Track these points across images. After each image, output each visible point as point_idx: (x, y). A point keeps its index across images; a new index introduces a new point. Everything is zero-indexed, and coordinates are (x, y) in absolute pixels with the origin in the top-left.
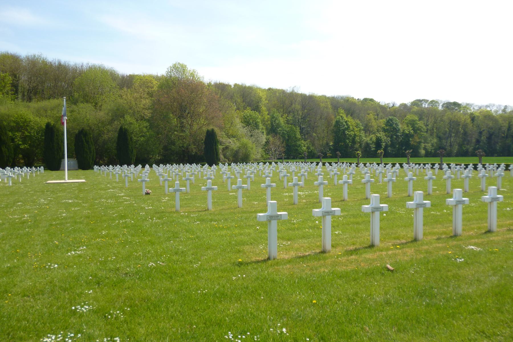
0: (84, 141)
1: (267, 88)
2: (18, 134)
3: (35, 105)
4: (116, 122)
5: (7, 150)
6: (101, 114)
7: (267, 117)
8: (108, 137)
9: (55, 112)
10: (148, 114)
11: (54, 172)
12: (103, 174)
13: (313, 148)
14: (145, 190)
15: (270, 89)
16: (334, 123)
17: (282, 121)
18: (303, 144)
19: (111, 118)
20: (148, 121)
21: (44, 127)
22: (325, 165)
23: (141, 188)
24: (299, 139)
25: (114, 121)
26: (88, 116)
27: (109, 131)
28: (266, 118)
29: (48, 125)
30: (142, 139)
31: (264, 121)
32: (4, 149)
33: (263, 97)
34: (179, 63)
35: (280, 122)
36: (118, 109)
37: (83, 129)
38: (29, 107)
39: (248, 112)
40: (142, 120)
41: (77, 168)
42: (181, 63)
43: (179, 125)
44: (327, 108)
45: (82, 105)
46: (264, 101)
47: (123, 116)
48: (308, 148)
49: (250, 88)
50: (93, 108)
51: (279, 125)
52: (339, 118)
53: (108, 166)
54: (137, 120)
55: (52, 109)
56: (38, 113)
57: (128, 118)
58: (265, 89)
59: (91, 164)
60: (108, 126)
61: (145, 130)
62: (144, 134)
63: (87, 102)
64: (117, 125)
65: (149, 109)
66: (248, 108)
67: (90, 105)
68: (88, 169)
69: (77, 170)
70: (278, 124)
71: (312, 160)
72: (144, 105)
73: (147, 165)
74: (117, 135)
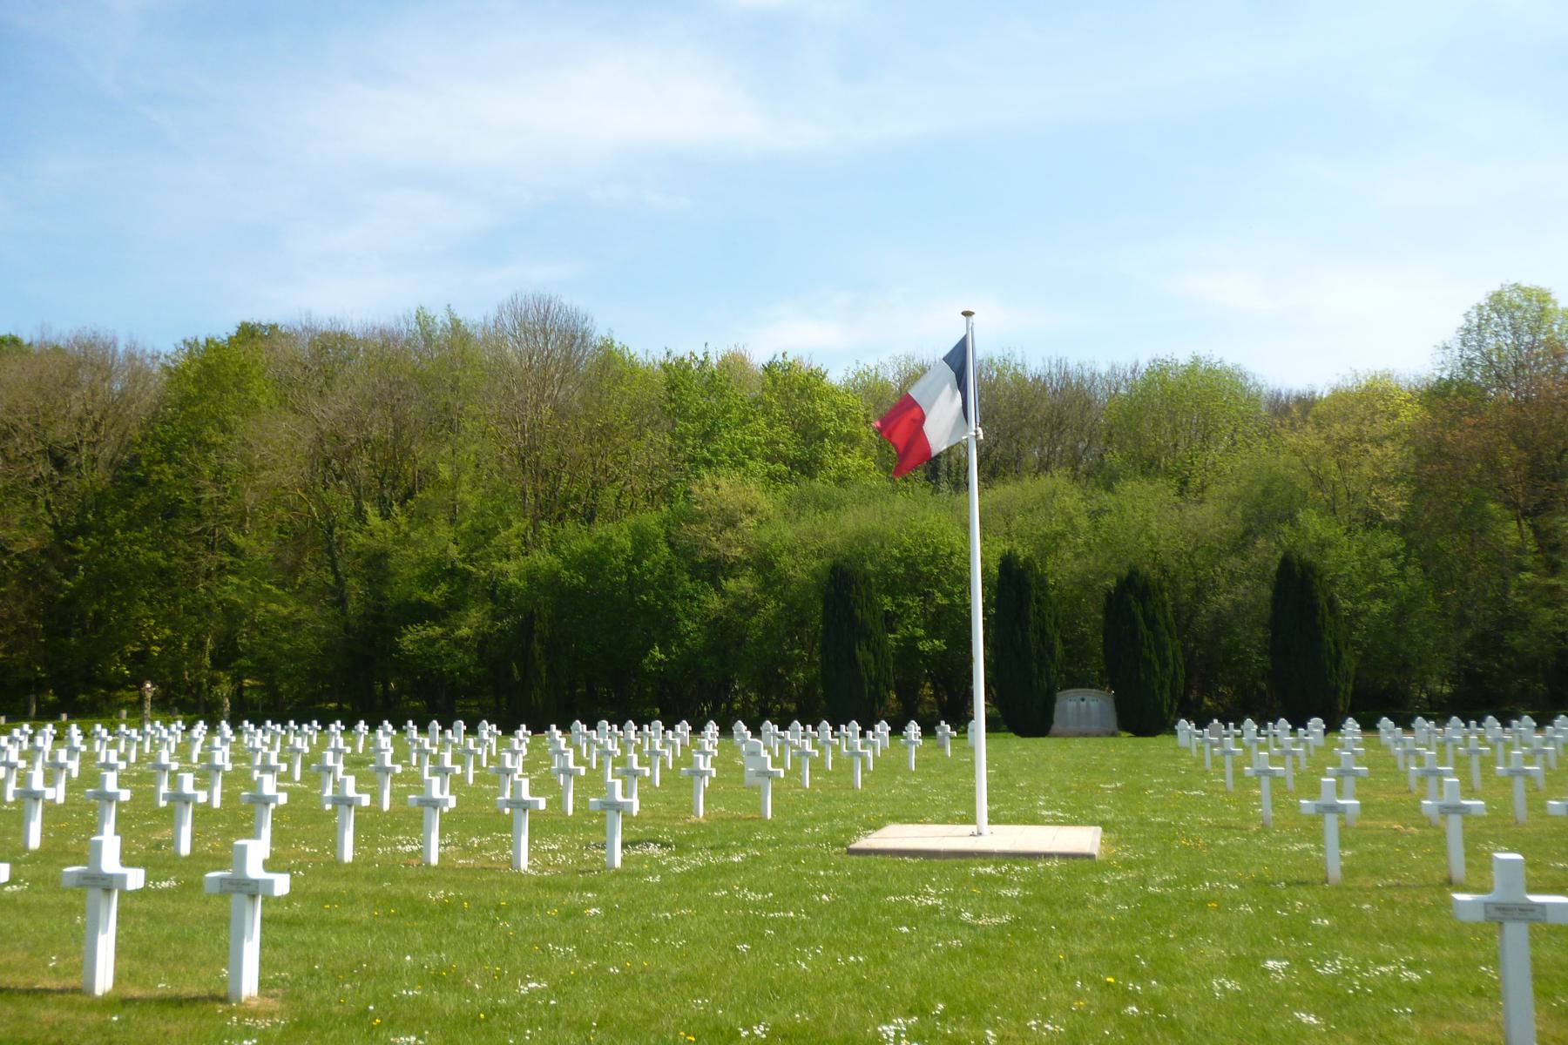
5: (871, 657)
30: (1377, 607)
32: (862, 654)
59: (1166, 711)
64: (1266, 553)
67: (1160, 482)
69: (1113, 734)
72: (1376, 467)
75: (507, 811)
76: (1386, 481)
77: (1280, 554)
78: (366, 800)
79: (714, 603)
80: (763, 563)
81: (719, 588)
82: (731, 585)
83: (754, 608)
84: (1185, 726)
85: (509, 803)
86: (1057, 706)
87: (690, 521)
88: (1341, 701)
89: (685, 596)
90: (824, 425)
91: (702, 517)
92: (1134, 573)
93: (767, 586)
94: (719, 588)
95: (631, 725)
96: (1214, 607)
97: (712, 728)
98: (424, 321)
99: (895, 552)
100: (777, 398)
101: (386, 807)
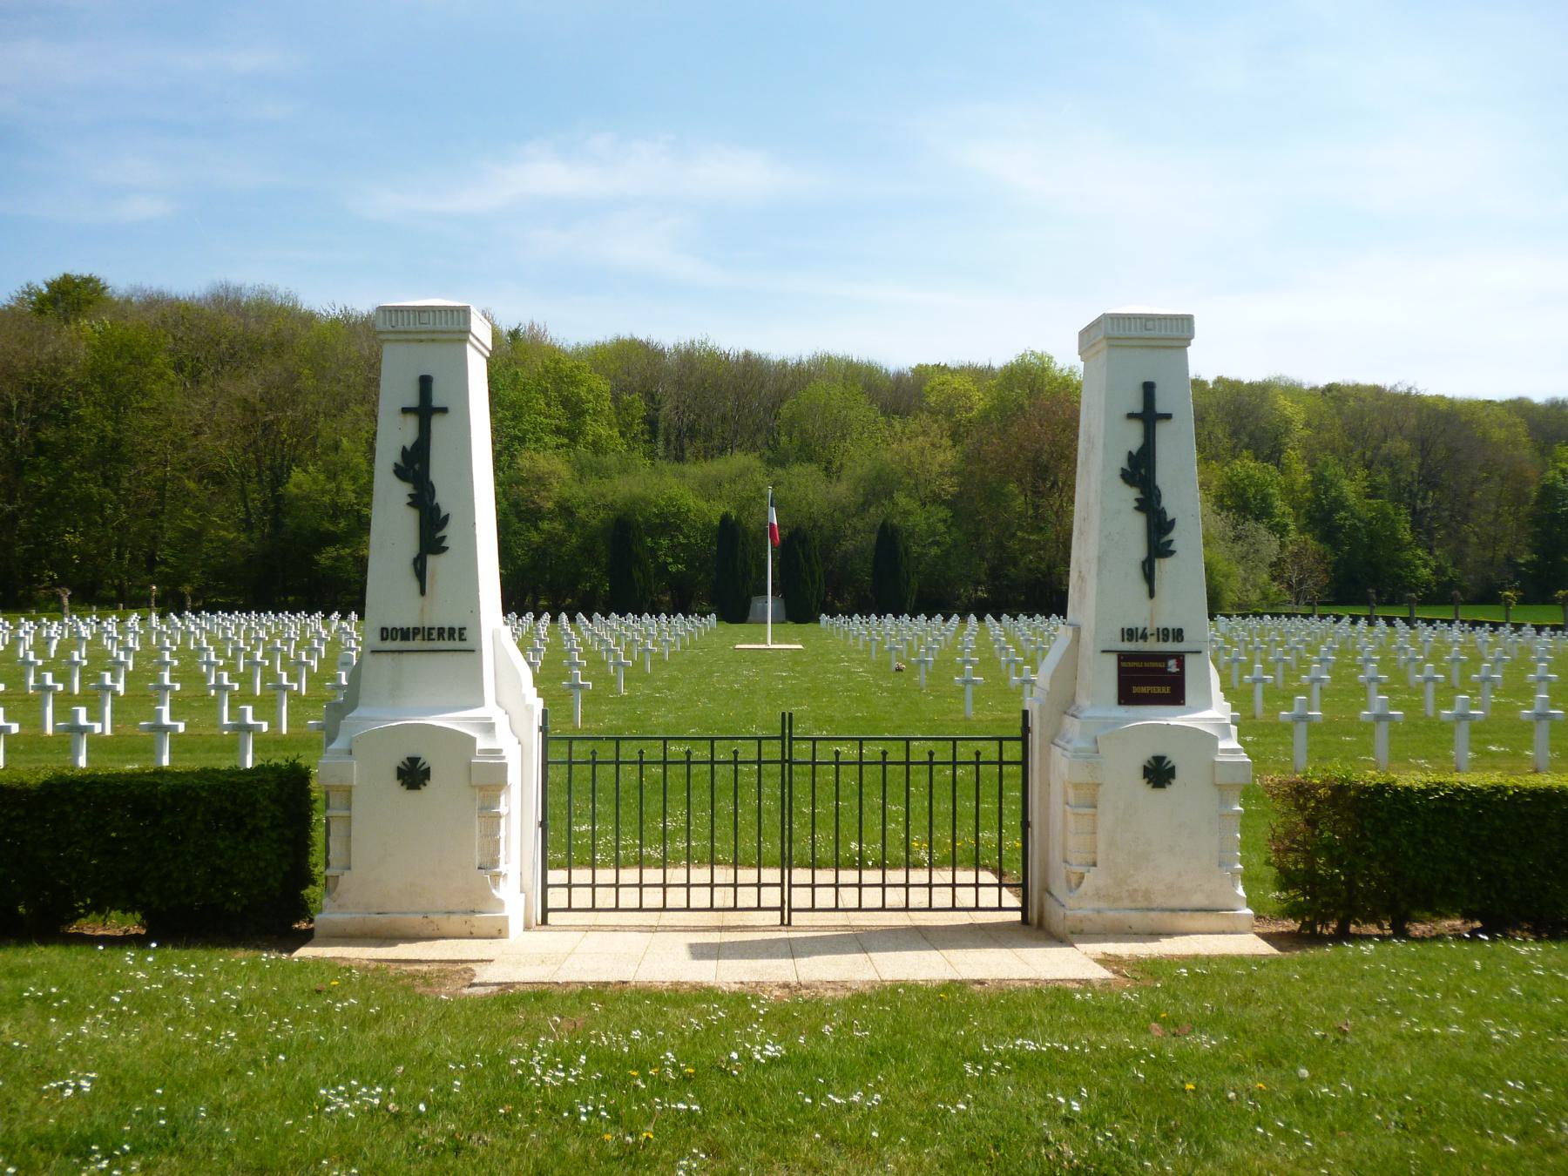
0: (801, 555)
1: (1322, 383)
2: (665, 542)
3: (697, 470)
4: (872, 510)
5: (641, 575)
6: (841, 490)
7: (1302, 477)
8: (854, 545)
9: (739, 487)
10: (950, 487)
11: (736, 627)
12: (838, 634)
13: (1457, 572)
14: (895, 664)
15: (1330, 388)
16: (1534, 492)
17: (1350, 489)
18: (1420, 559)
19: (862, 500)
20: (948, 504)
21: (716, 523)
22: (1393, 626)
23: (889, 664)
24: (1410, 543)
25: (870, 506)
26: (811, 497)
27: (856, 531)
28: (1301, 480)
29: (725, 519)
30: (934, 551)
31: (1293, 491)
32: (636, 574)
33: (1297, 418)
34: (1033, 353)
35: (1342, 493)
36: (878, 477)
37: (798, 529)
38: (683, 476)
39: (1246, 466)
40: (934, 501)
41: (783, 618)
42: (1039, 351)
43: (1031, 512)
44: (1515, 444)
45: (797, 469)
46: (1300, 431)
47: (889, 495)
48: (1438, 571)
49: (1262, 391)
50: (822, 474)
51: (1339, 504)
52: (1554, 478)
53: (248, 613)
54: (924, 504)
55: (732, 481)
56: (708, 489)
57: (901, 499)
58: (1314, 389)
59: (813, 609)
60: (855, 520)
61: (941, 527)
62: (938, 538)
63: (810, 459)
64: (875, 514)
65: (952, 474)
66: (1245, 453)
67: (814, 467)
68: (806, 622)
69: (783, 623)
70: (1335, 499)
71: (1338, 610)
72: (941, 466)
73: (972, 615)
74: (874, 538)
75: (213, 692)
76: (944, 474)
77: (883, 517)
78: (60, 687)
79: (535, 538)
80: (565, 510)
81: (537, 529)
82: (545, 525)
83: (561, 542)
84: (824, 617)
85: (215, 687)
86: (752, 606)
87: (517, 484)
88: (908, 605)
89: (515, 533)
90: (586, 406)
91: (527, 481)
92: (798, 529)
93: (570, 527)
94: (537, 529)
95: (663, 616)
96: (843, 548)
97: (547, 616)
98: (1170, 783)
99: (655, 510)
100: (551, 383)
101: (76, 691)
